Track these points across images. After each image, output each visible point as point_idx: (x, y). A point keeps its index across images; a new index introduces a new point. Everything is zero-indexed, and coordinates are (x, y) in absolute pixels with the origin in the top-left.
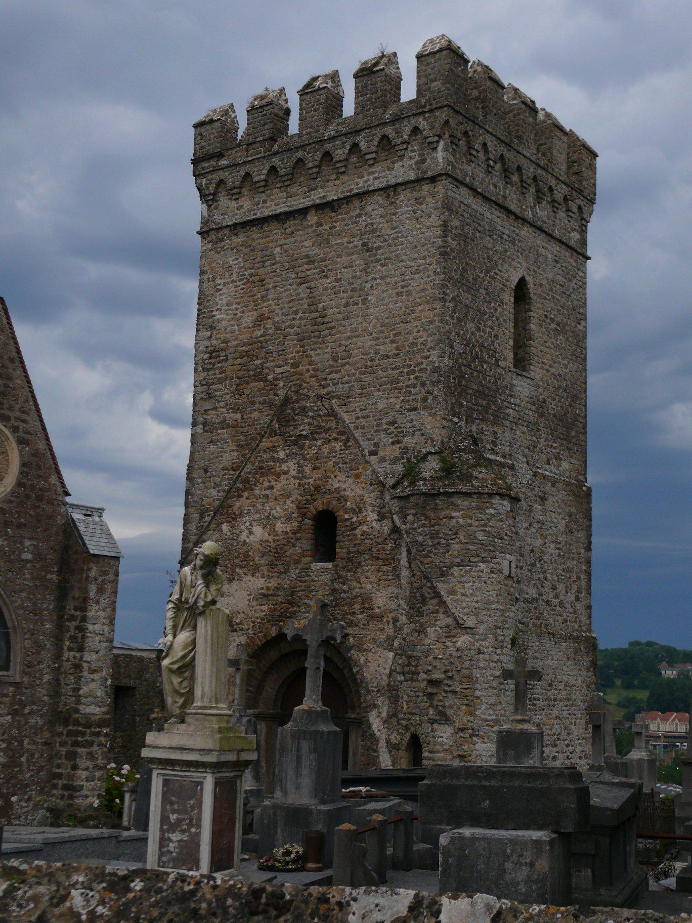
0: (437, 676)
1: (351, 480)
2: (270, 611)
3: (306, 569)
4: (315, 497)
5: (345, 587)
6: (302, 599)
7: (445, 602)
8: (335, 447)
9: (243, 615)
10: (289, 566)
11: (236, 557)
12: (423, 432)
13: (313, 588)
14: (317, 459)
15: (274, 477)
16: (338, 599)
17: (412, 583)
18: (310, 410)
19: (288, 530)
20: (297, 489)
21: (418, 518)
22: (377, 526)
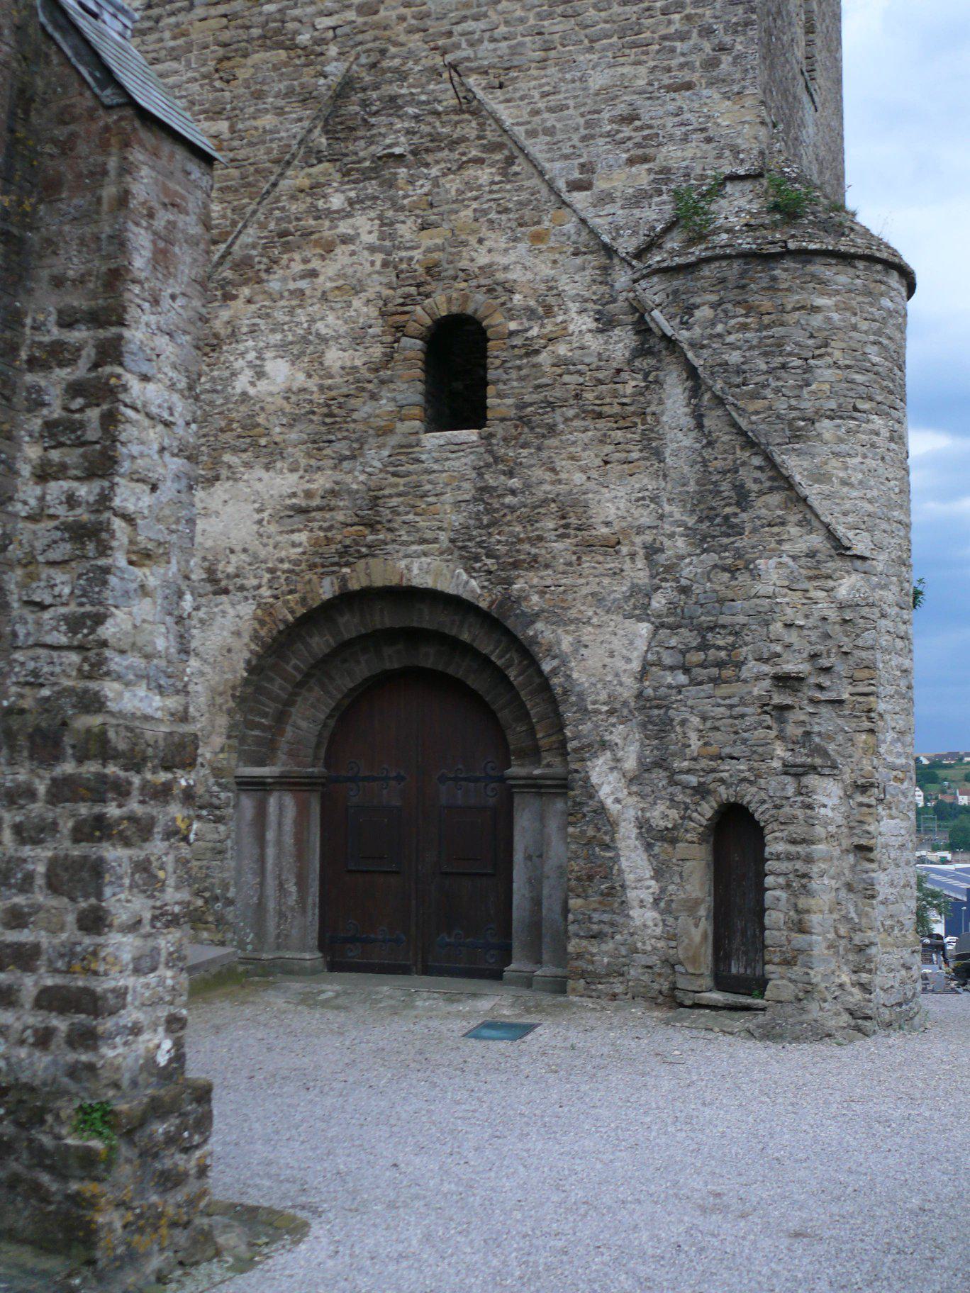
0: (792, 666)
1: (522, 247)
2: (316, 543)
3: (408, 448)
4: (428, 288)
5: (514, 483)
6: (399, 514)
7: (804, 500)
8: (477, 178)
9: (243, 557)
10: (362, 442)
11: (222, 430)
12: (711, 133)
13: (428, 487)
14: (431, 205)
15: (319, 251)
16: (496, 511)
17: (705, 463)
18: (409, 103)
19: (358, 363)
20: (379, 273)
21: (725, 312)
22: (594, 343)
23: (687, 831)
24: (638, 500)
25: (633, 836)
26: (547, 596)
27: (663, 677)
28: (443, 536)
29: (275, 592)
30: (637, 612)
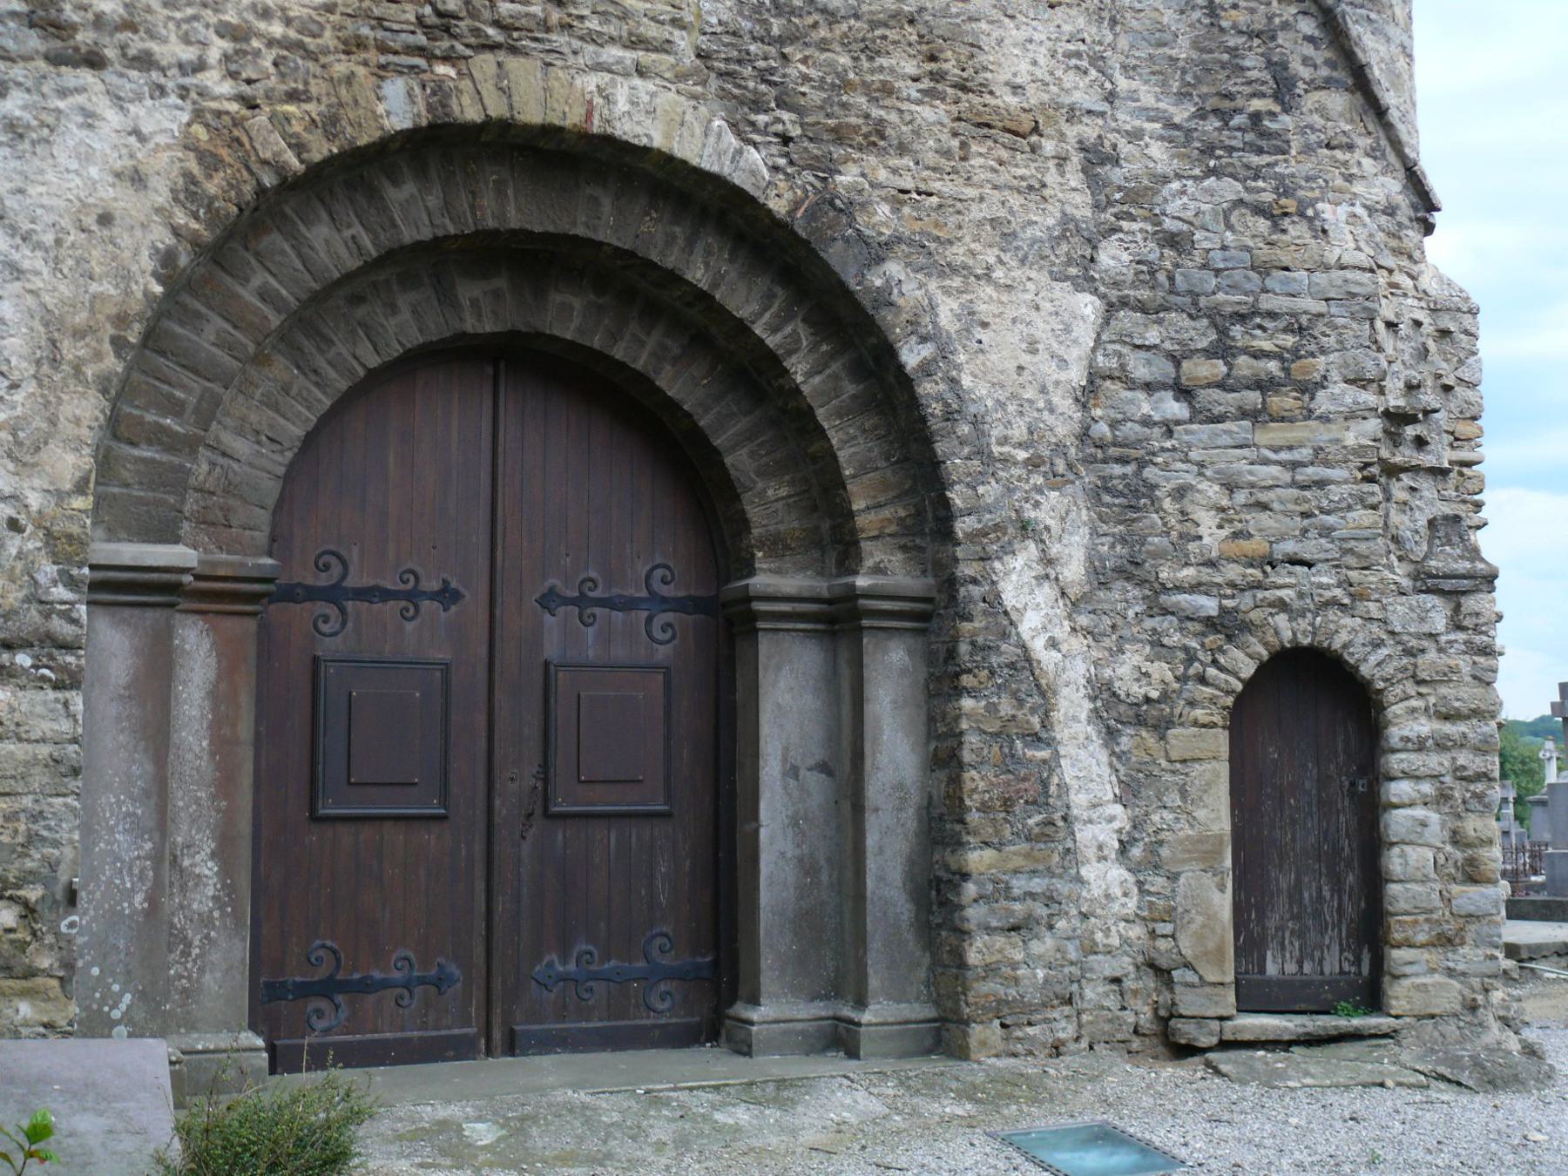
23: (1192, 704)
24: (1069, 55)
25: (1083, 716)
26: (906, 210)
27: (1131, 402)
28: (684, 42)
29: (247, 90)
30: (1073, 271)
